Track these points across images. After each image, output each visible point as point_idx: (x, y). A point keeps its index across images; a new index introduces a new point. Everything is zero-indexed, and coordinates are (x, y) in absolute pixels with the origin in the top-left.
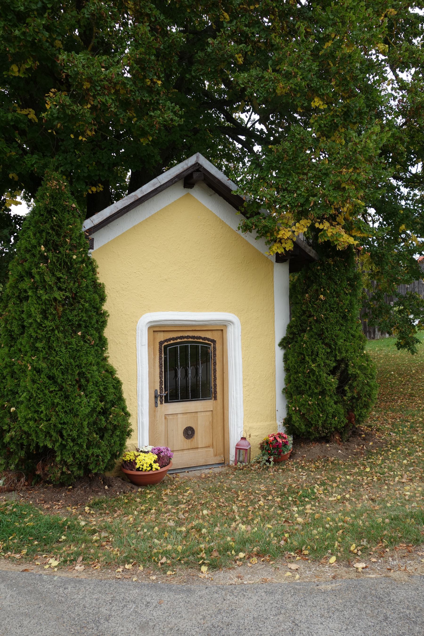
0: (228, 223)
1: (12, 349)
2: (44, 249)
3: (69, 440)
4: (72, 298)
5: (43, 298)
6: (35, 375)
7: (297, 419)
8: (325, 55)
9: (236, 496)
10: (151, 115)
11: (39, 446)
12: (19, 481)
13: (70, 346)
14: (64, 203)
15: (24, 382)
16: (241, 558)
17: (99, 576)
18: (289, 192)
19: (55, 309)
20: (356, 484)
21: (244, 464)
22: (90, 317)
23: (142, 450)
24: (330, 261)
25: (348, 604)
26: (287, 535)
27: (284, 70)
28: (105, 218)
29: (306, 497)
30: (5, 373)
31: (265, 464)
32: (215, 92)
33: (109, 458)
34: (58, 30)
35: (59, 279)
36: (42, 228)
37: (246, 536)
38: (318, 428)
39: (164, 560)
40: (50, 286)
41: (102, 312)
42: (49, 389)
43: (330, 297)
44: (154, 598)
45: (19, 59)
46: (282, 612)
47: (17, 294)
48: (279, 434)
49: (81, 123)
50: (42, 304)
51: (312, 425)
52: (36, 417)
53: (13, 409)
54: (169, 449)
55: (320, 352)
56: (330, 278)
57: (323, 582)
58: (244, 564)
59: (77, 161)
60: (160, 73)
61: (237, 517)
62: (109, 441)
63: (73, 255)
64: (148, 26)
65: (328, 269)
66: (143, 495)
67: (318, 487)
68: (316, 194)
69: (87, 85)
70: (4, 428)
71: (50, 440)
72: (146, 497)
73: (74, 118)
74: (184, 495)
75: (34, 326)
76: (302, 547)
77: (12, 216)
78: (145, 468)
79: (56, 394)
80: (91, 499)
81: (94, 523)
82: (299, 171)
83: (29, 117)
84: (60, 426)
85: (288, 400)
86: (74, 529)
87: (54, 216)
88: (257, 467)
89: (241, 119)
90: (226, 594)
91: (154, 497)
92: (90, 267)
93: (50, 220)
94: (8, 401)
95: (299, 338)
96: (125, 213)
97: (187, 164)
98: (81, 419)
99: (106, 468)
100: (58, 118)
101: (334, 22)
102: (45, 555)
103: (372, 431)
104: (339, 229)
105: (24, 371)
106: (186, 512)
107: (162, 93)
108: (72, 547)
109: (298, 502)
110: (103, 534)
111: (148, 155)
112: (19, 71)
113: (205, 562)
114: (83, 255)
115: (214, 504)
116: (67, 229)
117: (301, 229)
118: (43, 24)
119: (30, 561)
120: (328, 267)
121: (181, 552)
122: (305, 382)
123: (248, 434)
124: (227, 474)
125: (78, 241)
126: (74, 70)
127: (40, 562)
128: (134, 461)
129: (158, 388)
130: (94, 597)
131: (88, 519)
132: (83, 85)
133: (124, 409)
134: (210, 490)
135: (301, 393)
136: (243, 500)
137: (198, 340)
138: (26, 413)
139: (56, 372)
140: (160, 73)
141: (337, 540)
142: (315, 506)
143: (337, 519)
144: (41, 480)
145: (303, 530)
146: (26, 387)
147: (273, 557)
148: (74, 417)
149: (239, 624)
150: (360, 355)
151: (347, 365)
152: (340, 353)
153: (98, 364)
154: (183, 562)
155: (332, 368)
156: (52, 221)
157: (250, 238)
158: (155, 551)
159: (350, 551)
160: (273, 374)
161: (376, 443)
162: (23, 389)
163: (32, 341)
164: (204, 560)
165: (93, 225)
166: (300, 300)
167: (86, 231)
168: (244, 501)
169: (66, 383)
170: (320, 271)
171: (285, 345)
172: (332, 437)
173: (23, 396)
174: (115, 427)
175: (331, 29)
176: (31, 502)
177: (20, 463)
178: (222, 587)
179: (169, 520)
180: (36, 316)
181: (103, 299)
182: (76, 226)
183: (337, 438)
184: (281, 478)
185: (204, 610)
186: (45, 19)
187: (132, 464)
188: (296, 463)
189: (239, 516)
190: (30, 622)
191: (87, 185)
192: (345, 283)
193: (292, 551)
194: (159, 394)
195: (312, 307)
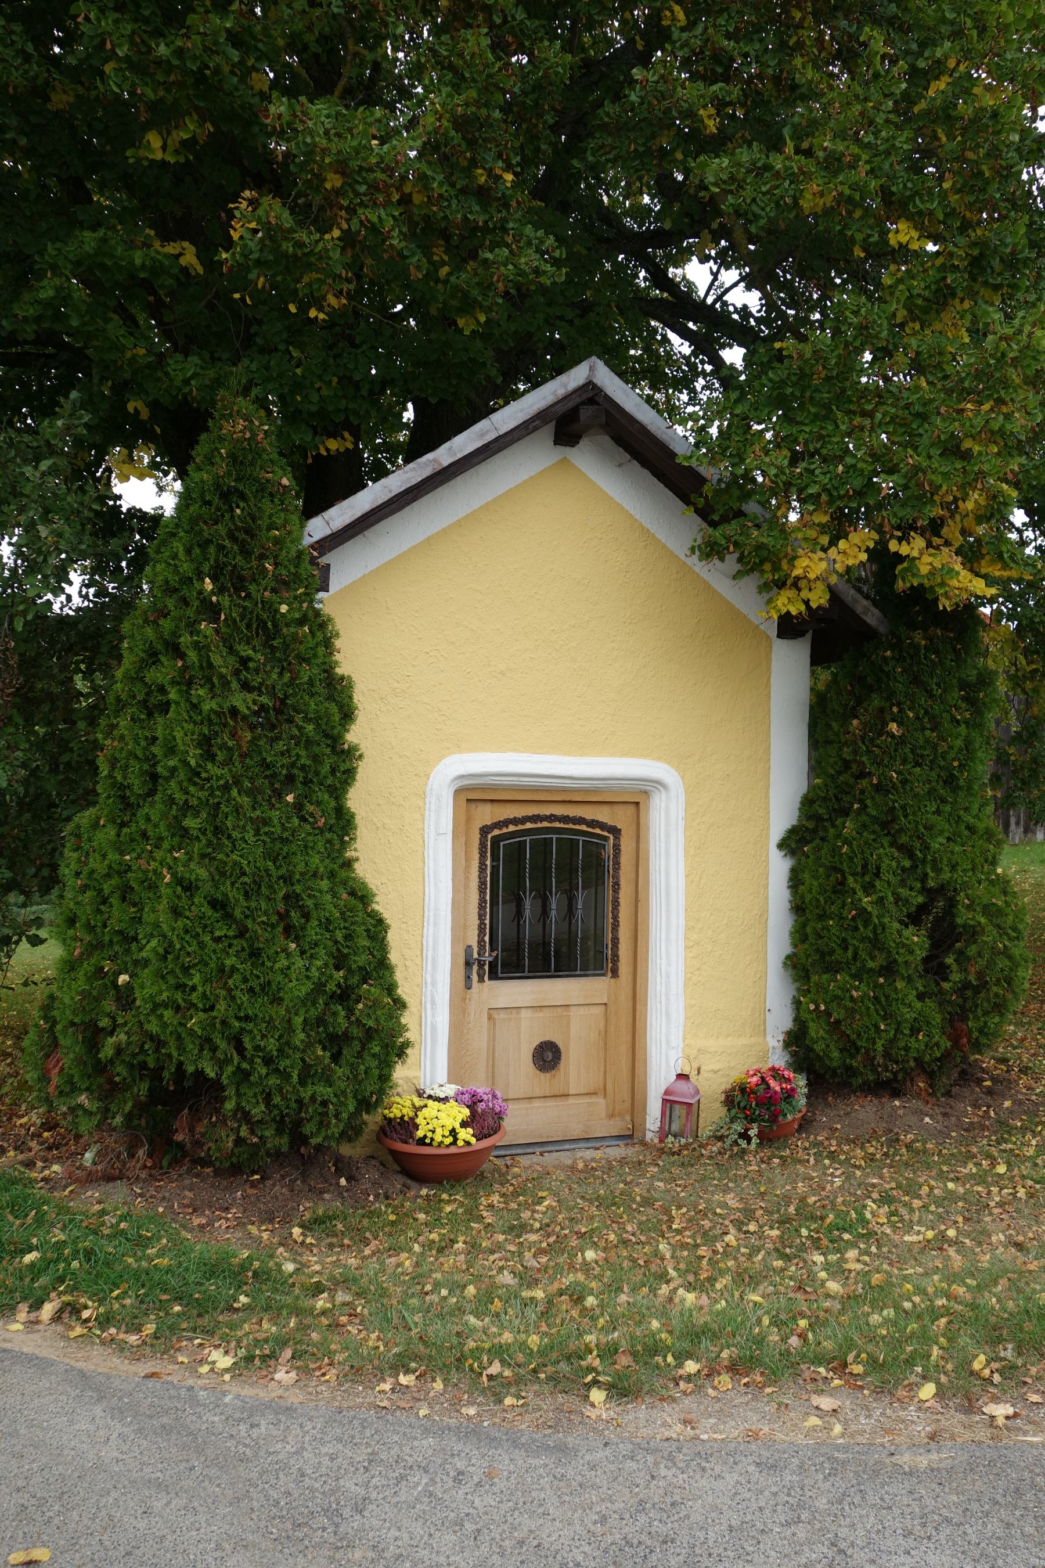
0: (661, 536)
1: (126, 830)
2: (211, 587)
3: (258, 1060)
4: (274, 709)
5: (206, 707)
6: (179, 898)
7: (821, 1033)
8: (928, 112)
9: (665, 1218)
10: (486, 260)
11: (185, 1071)
12: (132, 1155)
13: (266, 829)
14: (263, 474)
15: (154, 911)
16: (689, 1375)
17: (333, 1398)
19: (233, 735)
20: (971, 1204)
21: (683, 1141)
22: (316, 758)
23: (432, 1093)
24: (919, 638)
25: (975, 1506)
26: (803, 1323)
27: (825, 149)
28: (359, 514)
29: (845, 1230)
30: (107, 888)
31: (736, 1142)
32: (626, 213)
33: (351, 1109)
34: (260, 45)
35: (244, 661)
36: (206, 535)
37: (701, 1320)
38: (874, 1058)
39: (495, 1368)
40: (222, 677)
41: (346, 746)
42: (212, 932)
43: (916, 730)
44: (473, 1461)
45: (164, 116)
46: (803, 1517)
47: (140, 697)
48: (773, 1069)
49: (315, 275)
50: (202, 723)
51: (858, 1049)
52: (180, 1001)
53: (123, 978)
54: (499, 1094)
55: (884, 866)
56: (916, 681)
57: (905, 1447)
58: (699, 1389)
59: (295, 374)
60: (512, 155)
61: (673, 1273)
62: (353, 1067)
63: (280, 603)
64: (487, 34)
65: (911, 657)
66: (432, 1205)
67: (874, 1206)
68: (897, 465)
69: (333, 181)
70: (101, 1024)
71: (211, 1059)
72: (440, 1210)
73: (297, 263)
74: (534, 1211)
75: (182, 775)
76: (846, 1355)
77: (124, 510)
78: (438, 1138)
79: (230, 946)
80: (307, 1208)
81: (317, 1267)
82: (853, 407)
83: (183, 261)
84: (237, 1024)
85: (797, 984)
86: (268, 1279)
87: (238, 507)
88: (715, 1149)
89: (688, 282)
90: (656, 1464)
91: (460, 1211)
92: (319, 636)
93: (227, 516)
94: (113, 959)
95: (832, 831)
96: (408, 504)
97: (565, 386)
98: (287, 1010)
99: (342, 1134)
100: (258, 263)
101: (956, 28)
102: (198, 1341)
103: (1008, 1071)
104: (947, 557)
105: (153, 887)
106: (541, 1252)
107: (514, 204)
108: (265, 1325)
109: (825, 1242)
110: (341, 1297)
111: (470, 359)
112: (164, 148)
113: (600, 1378)
114: (305, 605)
115: (612, 1237)
116: (268, 539)
117: (854, 550)
118: (228, 30)
119: (164, 1353)
120: (911, 651)
121: (539, 1351)
122: (844, 940)
123: (695, 1066)
124: (640, 1163)
125: (293, 570)
126: (304, 142)
127: (188, 1356)
128: (412, 1119)
129: (474, 943)
130: (325, 1450)
131: (300, 1257)
132: (325, 180)
133: (391, 989)
134: (601, 1202)
135: (833, 969)
136: (685, 1229)
137: (577, 827)
138: (156, 988)
139: (231, 892)
140: (512, 155)
141: (937, 1343)
142: (868, 1253)
143: (930, 1290)
144: (184, 1157)
145: (843, 1311)
146: (157, 925)
147: (773, 1377)
148: (271, 1003)
149: (692, 1541)
150: (987, 879)
151: (952, 903)
152: (938, 870)
153: (332, 875)
154: (543, 1376)
155: (913, 909)
156: (232, 517)
157: (717, 576)
158: (472, 1344)
159: (972, 1373)
160: (763, 916)
161: (1020, 1103)
162: (149, 929)
163: (174, 812)
164: (598, 1373)
165: (329, 532)
166: (837, 735)
167: (312, 546)
168: (687, 1233)
169: (254, 920)
170: (892, 663)
171: (793, 845)
172: (908, 1084)
173: (148, 947)
174: (370, 1034)
175: (948, 44)
176: (161, 1210)
177: (136, 1112)
178: (644, 1445)
179: (501, 1269)
180: (187, 752)
181: (348, 715)
182: (289, 533)
183: (921, 1085)
184: (779, 1180)
185: (603, 1500)
186: (232, 16)
187: (406, 1127)
188: (816, 1144)
189: (675, 1269)
190: (168, 1503)
191: (315, 433)
192: (955, 695)
193: (820, 1365)
194: (476, 956)
195: (869, 752)
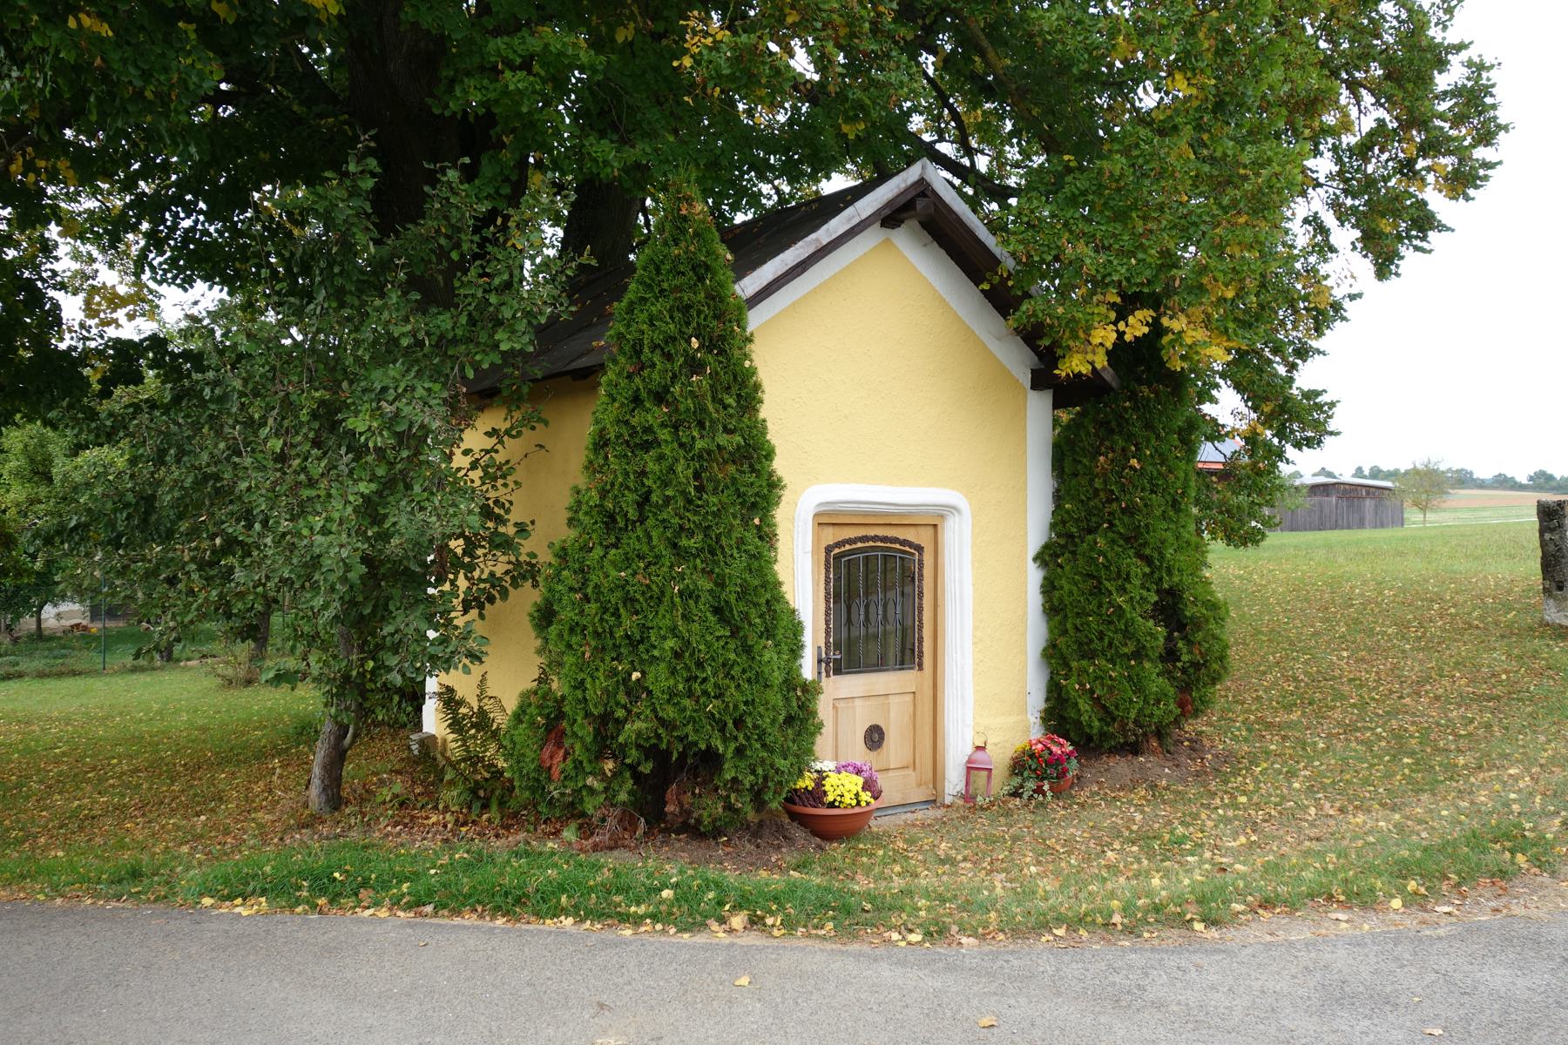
0: (954, 305)
18: (1122, 253)
53: (636, 675)
78: (847, 800)
135: (1090, 656)
187: (817, 795)
